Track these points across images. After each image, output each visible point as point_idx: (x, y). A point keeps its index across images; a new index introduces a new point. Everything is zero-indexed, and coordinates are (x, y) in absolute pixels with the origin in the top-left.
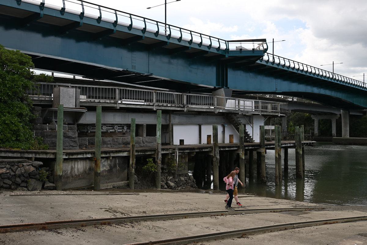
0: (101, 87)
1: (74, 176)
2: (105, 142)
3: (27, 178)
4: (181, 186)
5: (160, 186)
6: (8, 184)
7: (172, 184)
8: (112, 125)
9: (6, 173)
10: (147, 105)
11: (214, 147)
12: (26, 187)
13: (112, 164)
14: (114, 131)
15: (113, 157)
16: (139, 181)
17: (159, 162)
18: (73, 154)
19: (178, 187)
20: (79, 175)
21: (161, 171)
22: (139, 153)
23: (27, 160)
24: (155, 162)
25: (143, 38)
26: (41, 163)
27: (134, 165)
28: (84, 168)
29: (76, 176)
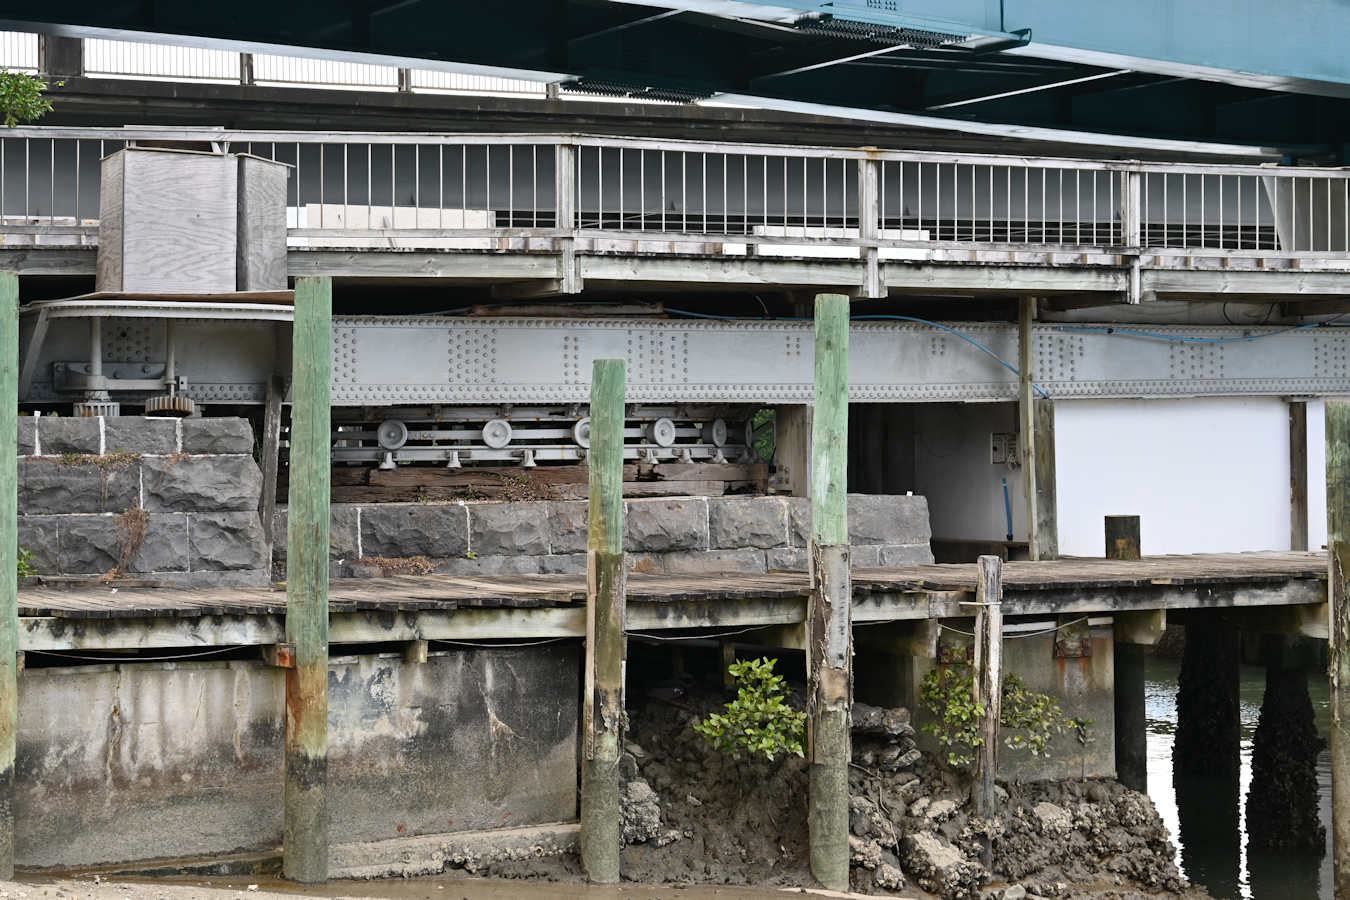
0: (440, 140)
1: (134, 777)
2: (494, 534)
4: (1033, 872)
5: (843, 870)
10: (695, 258)
11: (1336, 573)
13: (448, 694)
14: (568, 454)
15: (434, 645)
16: (669, 822)
17: (833, 679)
18: (107, 622)
20: (174, 775)
21: (846, 753)
22: (663, 616)
27: (613, 709)
29: (147, 781)
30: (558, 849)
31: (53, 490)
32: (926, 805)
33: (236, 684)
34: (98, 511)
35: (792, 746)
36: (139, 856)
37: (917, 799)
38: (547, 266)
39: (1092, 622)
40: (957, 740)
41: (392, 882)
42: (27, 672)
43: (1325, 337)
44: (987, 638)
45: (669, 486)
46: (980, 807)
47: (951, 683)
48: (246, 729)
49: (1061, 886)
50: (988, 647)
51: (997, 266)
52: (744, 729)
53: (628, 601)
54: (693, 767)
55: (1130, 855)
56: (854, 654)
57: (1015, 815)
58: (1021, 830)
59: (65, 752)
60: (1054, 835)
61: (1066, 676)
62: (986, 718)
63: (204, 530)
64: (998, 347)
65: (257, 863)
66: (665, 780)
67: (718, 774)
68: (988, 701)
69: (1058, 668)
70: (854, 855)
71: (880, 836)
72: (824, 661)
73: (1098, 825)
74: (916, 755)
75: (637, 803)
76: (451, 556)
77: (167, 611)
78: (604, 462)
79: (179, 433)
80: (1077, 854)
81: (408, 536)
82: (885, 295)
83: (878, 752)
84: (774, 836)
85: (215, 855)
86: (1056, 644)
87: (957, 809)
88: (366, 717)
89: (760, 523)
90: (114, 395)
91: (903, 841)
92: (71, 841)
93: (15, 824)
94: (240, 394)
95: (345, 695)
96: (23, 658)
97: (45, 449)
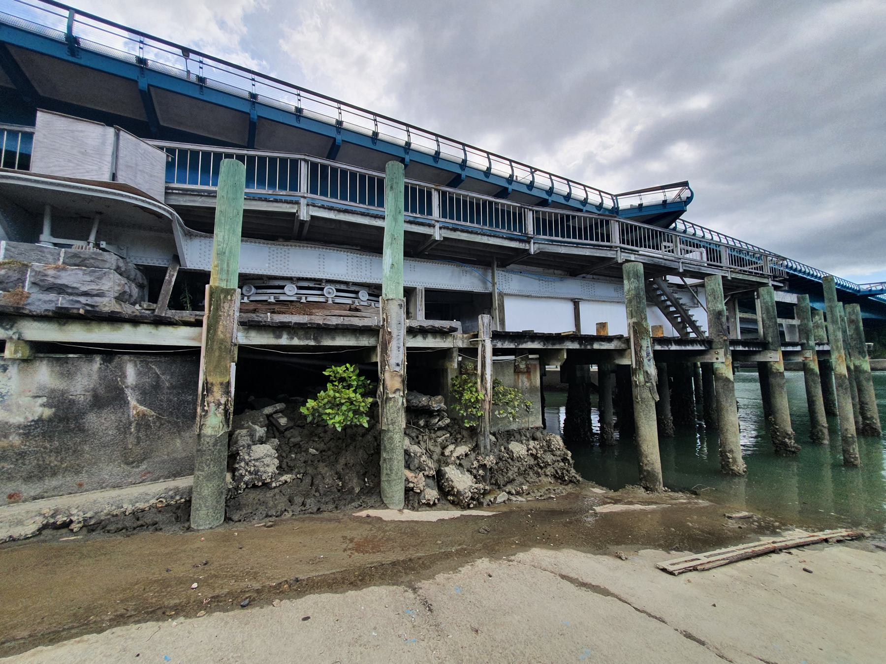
4: (511, 481)
5: (400, 495)
8: (318, 284)
14: (322, 299)
22: (280, 337)
30: (181, 498)
32: (453, 449)
35: (361, 420)
37: (448, 446)
38: (293, 208)
40: (469, 413)
44: (484, 357)
45: (364, 314)
46: (482, 449)
47: (465, 382)
49: (525, 487)
50: (485, 362)
55: (554, 466)
56: (406, 363)
57: (500, 451)
58: (504, 459)
60: (519, 459)
61: (520, 381)
62: (484, 400)
64: (485, 275)
67: (333, 434)
69: (516, 377)
70: (408, 484)
71: (425, 470)
72: (387, 367)
73: (539, 452)
74: (448, 421)
75: (256, 460)
80: (530, 468)
82: (442, 239)
83: (428, 420)
86: (515, 366)
87: (470, 451)
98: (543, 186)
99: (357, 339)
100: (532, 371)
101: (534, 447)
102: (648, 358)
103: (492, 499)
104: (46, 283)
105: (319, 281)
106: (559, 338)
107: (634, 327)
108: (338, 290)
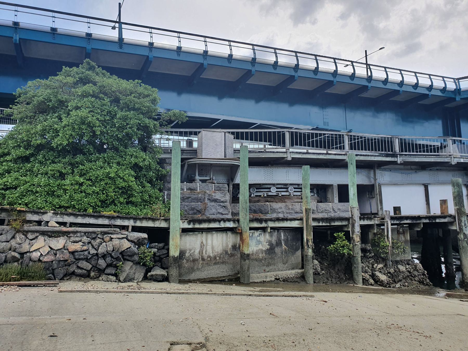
3: (118, 259)
4: (400, 281)
5: (361, 280)
6: (85, 270)
7: (383, 278)
8: (286, 186)
9: (81, 251)
12: (116, 275)
13: (274, 239)
14: (287, 194)
15: (272, 228)
16: (322, 269)
17: (357, 238)
19: (395, 282)
20: (215, 258)
21: (360, 254)
22: (319, 223)
23: (118, 230)
24: (348, 237)
25: (334, 84)
26: (145, 235)
27: (310, 243)
28: (224, 245)
31: (188, 198)
33: (228, 236)
34: (197, 202)
36: (207, 277)
39: (404, 226)
41: (263, 283)
42: (182, 233)
43: (431, 172)
44: (388, 228)
46: (388, 266)
48: (231, 247)
51: (372, 156)
52: (339, 248)
53: (312, 219)
54: (324, 257)
59: (191, 252)
60: (403, 272)
63: (218, 206)
65: (234, 279)
66: (319, 260)
68: (389, 243)
71: (368, 273)
74: (373, 254)
76: (266, 213)
77: (213, 219)
78: (306, 188)
79: (213, 187)
80: (408, 277)
81: (257, 209)
84: (344, 273)
85: (224, 277)
88: (256, 244)
89: (326, 208)
90: (201, 180)
91: (372, 273)
92: (192, 273)
93: (179, 270)
94: (224, 181)
95: (252, 239)
96: (181, 229)
97: (187, 189)
98: (393, 80)
99: (342, 222)
100: (406, 232)
101: (409, 268)
102: (465, 226)
103: (394, 286)
104: (213, 199)
105: (286, 185)
106: (419, 218)
107: (457, 211)
108: (295, 188)
